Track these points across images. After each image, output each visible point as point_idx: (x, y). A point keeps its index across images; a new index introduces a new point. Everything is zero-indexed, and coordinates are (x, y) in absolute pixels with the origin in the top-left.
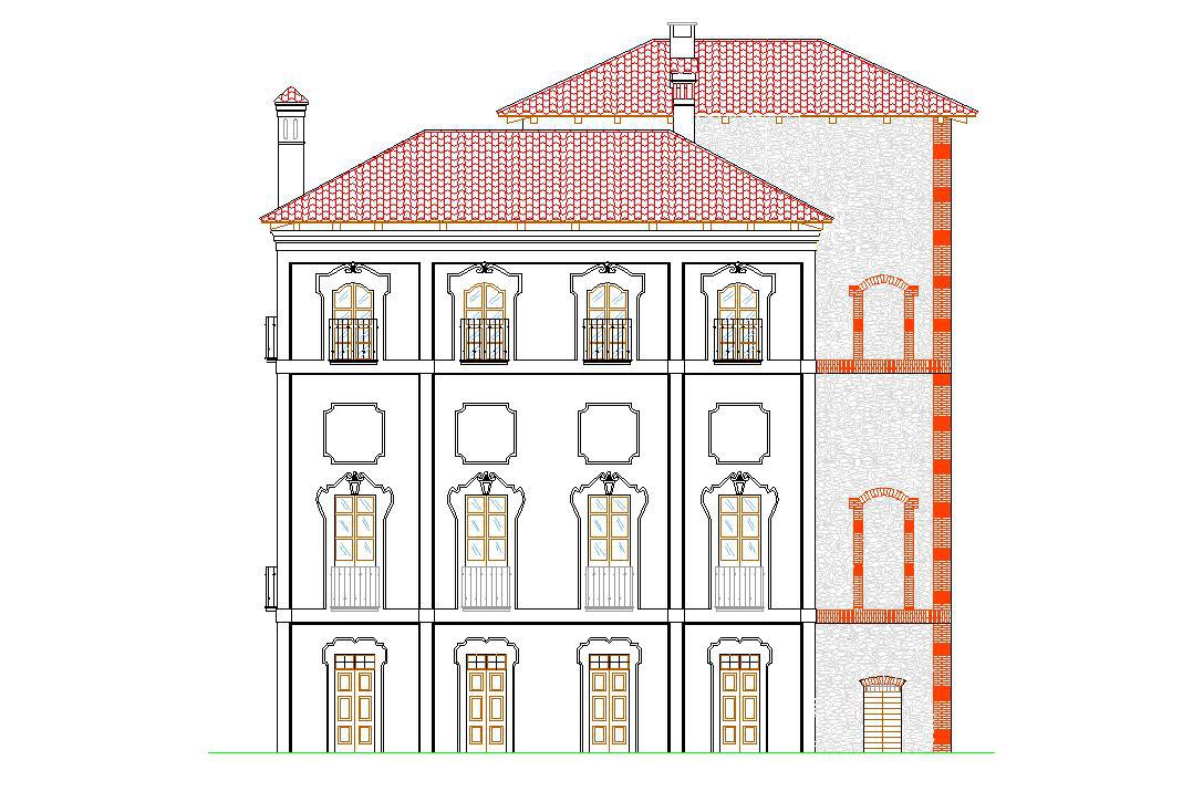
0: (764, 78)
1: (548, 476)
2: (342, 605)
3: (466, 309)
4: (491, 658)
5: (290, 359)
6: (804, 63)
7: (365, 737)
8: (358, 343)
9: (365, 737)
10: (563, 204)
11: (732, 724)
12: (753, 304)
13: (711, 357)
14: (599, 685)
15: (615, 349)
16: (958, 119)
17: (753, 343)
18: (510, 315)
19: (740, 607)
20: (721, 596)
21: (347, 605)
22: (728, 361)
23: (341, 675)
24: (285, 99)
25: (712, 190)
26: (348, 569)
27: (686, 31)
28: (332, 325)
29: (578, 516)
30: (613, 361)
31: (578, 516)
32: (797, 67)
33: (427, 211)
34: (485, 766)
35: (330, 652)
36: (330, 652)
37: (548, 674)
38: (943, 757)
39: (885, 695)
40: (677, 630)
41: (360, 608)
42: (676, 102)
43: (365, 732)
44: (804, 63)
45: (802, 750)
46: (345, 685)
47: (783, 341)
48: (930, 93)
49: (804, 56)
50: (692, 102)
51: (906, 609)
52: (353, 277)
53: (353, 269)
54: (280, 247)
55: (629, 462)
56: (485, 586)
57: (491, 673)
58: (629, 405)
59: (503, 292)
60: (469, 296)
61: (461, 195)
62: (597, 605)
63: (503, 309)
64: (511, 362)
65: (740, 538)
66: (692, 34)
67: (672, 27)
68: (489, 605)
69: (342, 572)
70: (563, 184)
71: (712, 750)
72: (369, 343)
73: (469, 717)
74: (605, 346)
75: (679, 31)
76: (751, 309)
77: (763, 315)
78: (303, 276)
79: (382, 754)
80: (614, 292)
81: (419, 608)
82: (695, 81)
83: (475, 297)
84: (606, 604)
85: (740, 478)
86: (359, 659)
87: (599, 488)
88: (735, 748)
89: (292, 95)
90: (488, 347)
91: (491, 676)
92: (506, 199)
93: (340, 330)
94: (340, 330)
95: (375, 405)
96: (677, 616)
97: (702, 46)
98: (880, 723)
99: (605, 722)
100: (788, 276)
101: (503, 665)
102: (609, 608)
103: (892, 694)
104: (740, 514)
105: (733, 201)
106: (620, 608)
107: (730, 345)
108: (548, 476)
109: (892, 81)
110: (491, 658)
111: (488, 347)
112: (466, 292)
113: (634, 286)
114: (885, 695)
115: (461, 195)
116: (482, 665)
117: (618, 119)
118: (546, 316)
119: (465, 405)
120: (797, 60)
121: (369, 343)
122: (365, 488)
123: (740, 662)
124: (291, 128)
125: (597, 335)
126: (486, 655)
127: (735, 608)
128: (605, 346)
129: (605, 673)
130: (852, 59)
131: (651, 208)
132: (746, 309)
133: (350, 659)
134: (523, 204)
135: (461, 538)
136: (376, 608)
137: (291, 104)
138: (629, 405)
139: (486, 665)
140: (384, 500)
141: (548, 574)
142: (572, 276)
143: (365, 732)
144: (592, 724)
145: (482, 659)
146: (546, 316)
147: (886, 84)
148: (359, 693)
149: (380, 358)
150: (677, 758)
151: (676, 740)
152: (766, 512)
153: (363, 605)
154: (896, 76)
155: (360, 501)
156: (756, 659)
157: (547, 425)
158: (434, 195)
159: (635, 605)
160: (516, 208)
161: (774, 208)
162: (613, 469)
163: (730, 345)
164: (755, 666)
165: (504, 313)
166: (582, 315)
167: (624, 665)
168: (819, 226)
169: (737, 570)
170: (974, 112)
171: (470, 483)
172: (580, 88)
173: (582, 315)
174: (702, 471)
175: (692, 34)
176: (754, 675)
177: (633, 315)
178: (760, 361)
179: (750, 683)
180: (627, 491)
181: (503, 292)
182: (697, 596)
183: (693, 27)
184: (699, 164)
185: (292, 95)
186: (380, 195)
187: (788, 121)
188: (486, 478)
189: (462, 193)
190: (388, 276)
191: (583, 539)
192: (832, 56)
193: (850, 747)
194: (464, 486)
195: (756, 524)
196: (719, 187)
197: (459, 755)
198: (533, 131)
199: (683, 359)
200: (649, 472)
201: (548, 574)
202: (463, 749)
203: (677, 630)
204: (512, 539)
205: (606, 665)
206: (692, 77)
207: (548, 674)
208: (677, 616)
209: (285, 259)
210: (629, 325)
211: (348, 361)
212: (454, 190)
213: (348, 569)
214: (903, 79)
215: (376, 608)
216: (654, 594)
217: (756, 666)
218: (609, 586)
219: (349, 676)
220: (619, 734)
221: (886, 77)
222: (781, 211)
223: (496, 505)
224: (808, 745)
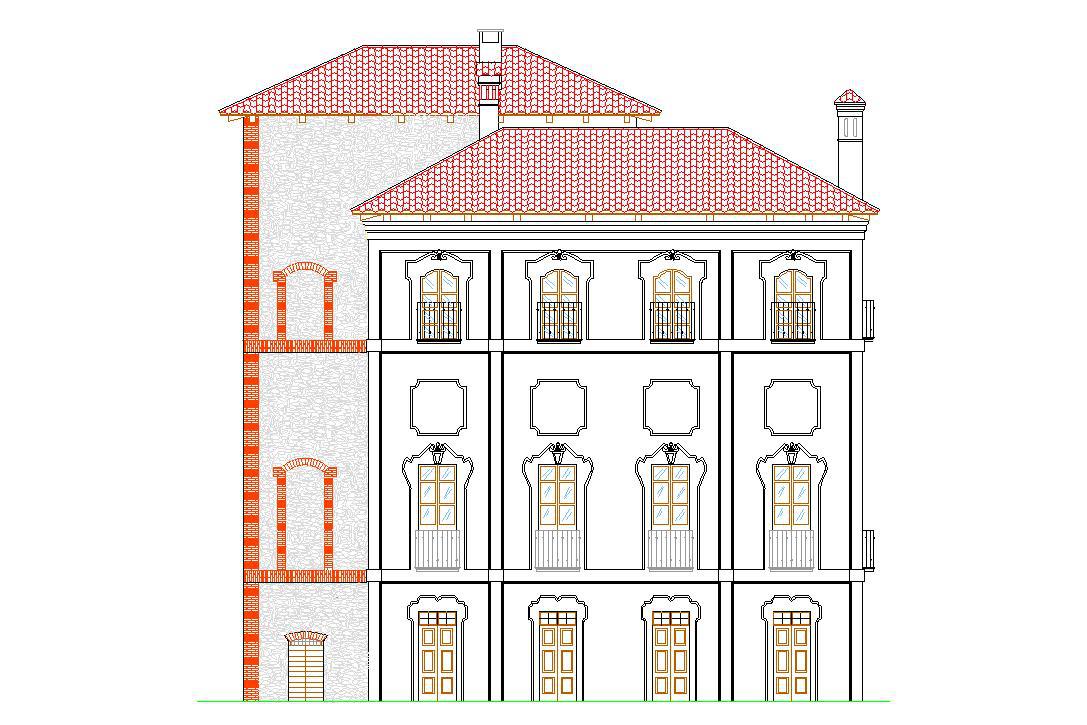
0: (528, 86)
1: (615, 447)
2: (435, 566)
3: (655, 293)
4: (442, 615)
5: (733, 338)
6: (390, 73)
7: (567, 688)
9: (567, 688)
10: (475, 197)
13: (768, 337)
14: (783, 639)
16: (644, 117)
18: (696, 299)
19: (662, 568)
20: (540, 560)
21: (794, 566)
22: (549, 340)
23: (424, 631)
24: (844, 99)
25: (750, 184)
26: (683, 533)
27: (493, 37)
28: (774, 308)
29: (641, 482)
30: (564, 340)
31: (641, 482)
32: (384, 77)
33: (662, 203)
35: (769, 609)
37: (614, 628)
39: (308, 648)
40: (496, 587)
41: (442, 568)
42: (482, 102)
44: (390, 73)
46: (661, 639)
48: (619, 94)
49: (390, 67)
50: (496, 102)
52: (559, 264)
53: (559, 257)
56: (557, 549)
57: (562, 627)
59: (690, 278)
61: (731, 188)
63: (689, 293)
64: (584, 341)
65: (670, 504)
66: (500, 40)
67: (481, 34)
68: (569, 566)
69: (678, 536)
70: (475, 178)
71: (645, 699)
73: (542, 669)
74: (669, 329)
75: (488, 37)
77: (583, 299)
78: (394, 264)
82: (500, 83)
84: (555, 566)
85: (671, 449)
86: (561, 615)
87: (428, 458)
88: (553, 697)
89: (850, 96)
90: (561, 329)
91: (796, 631)
92: (497, 192)
93: (661, 312)
94: (661, 312)
95: (766, 388)
96: (496, 576)
97: (510, 51)
98: (303, 680)
99: (665, 671)
100: (838, 263)
101: (686, 622)
102: (438, 568)
103: (314, 651)
104: (557, 482)
105: (818, 194)
106: (671, 568)
108: (615, 447)
109: (596, 89)
110: (674, 615)
111: (561, 329)
112: (655, 278)
114: (308, 648)
115: (731, 188)
116: (434, 622)
117: (550, 118)
118: (616, 303)
120: (384, 70)
122: (802, 458)
123: (438, 618)
124: (850, 127)
125: (430, 317)
127: (787, 568)
128: (669, 329)
129: (665, 627)
130: (560, 70)
131: (718, 200)
132: (448, 293)
133: (788, 615)
134: (712, 196)
135: (534, 505)
136: (811, 569)
137: (850, 104)
139: (671, 622)
140: (818, 468)
141: (614, 540)
142: (640, 262)
145: (434, 615)
146: (616, 303)
147: (590, 92)
149: (463, 337)
150: (496, 706)
151: (496, 689)
153: (799, 566)
154: (600, 85)
155: (797, 470)
156: (573, 615)
157: (616, 404)
158: (768, 188)
159: (582, 566)
160: (706, 200)
161: (731, 200)
164: (685, 622)
165: (691, 297)
166: (536, 298)
167: (685, 622)
168: (866, 217)
170: (223, 112)
171: (423, 453)
172: (284, 95)
173: (536, 298)
174: (522, 443)
175: (500, 40)
176: (451, 631)
177: (583, 299)
178: (580, 341)
179: (680, 636)
180: (807, 460)
181: (690, 278)
182: (516, 556)
183: (500, 34)
184: (568, 156)
185: (850, 96)
186: (794, 188)
187: (415, 122)
188: (792, 449)
189: (731, 187)
190: (825, 262)
191: (647, 506)
192: (540, 67)
193: (276, 696)
194: (771, 457)
195: (777, 496)
196: (756, 181)
198: (647, 129)
199: (502, 338)
200: (472, 443)
201: (614, 540)
203: (496, 587)
204: (582, 506)
205: (554, 622)
206: (496, 79)
207: (614, 628)
208: (496, 576)
209: (375, 247)
211: (667, 340)
212: (724, 184)
213: (683, 533)
214: (606, 87)
215: (811, 569)
216: (477, 558)
217: (686, 622)
218: (671, 549)
219: (666, 631)
221: (590, 85)
222: (738, 203)
223: (446, 473)
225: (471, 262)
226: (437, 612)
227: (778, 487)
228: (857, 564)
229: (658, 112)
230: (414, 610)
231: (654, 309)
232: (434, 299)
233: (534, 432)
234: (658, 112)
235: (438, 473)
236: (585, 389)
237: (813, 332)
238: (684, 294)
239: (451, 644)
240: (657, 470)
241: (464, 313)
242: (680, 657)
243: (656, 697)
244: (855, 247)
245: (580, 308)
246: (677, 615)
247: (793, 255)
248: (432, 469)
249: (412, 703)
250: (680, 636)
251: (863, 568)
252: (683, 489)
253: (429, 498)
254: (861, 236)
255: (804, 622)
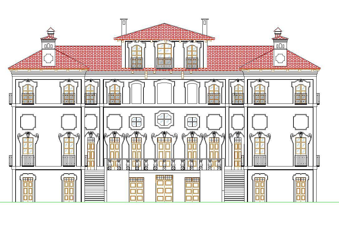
7: (31, 199)
8: (27, 99)
11: (67, 195)
12: (72, 90)
13: (253, 103)
15: (71, 101)
17: (213, 99)
26: (31, 156)
28: (208, 95)
34: (140, 205)
35: (22, 177)
36: (63, 177)
38: (28, 206)
43: (31, 197)
45: (81, 201)
47: (126, 100)
51: (220, 168)
54: (13, 75)
55: (74, 129)
58: (33, 115)
60: (297, 87)
62: (259, 165)
63: (219, 91)
69: (30, 157)
72: (32, 99)
74: (68, 101)
76: (241, 91)
79: (308, 203)
80: (117, 87)
81: (313, 166)
83: (66, 88)
86: (302, 179)
90: (261, 101)
95: (265, 115)
99: (68, 194)
104: (28, 142)
107: (304, 100)
110: (302, 179)
111: (261, 101)
113: (121, 85)
119: (35, 117)
121: (32, 99)
125: (212, 97)
126: (28, 178)
128: (68, 101)
133: (300, 179)
138: (33, 115)
143: (262, 197)
144: (297, 195)
148: (300, 187)
152: (266, 142)
162: (70, 131)
163: (304, 100)
164: (305, 180)
167: (305, 180)
169: (259, 156)
176: (72, 183)
179: (30, 184)
180: (32, 136)
197: (21, 203)
202: (22, 201)
205: (300, 180)
209: (14, 78)
210: (121, 95)
213: (31, 156)
217: (264, 180)
220: (303, 198)
224: (315, 200)
225: (123, 82)
226: (301, 178)
227: (24, 144)
228: (83, 165)
229: (213, 39)
230: (295, 177)
231: (63, 95)
232: (68, 92)
233: (130, 129)
234: (213, 39)
235: (28, 140)
236: (296, 115)
237: (33, 101)
238: (241, 91)
239: (263, 186)
240: (297, 139)
241: (308, 96)
242: (303, 190)
243: (24, 201)
244: (314, 78)
245: (34, 95)
246: (30, 179)
247: (260, 80)
248: (68, 139)
249: (294, 203)
250: (30, 184)
251: (317, 166)
252: (263, 144)
253: (26, 147)
254: (316, 75)
255: (263, 180)
